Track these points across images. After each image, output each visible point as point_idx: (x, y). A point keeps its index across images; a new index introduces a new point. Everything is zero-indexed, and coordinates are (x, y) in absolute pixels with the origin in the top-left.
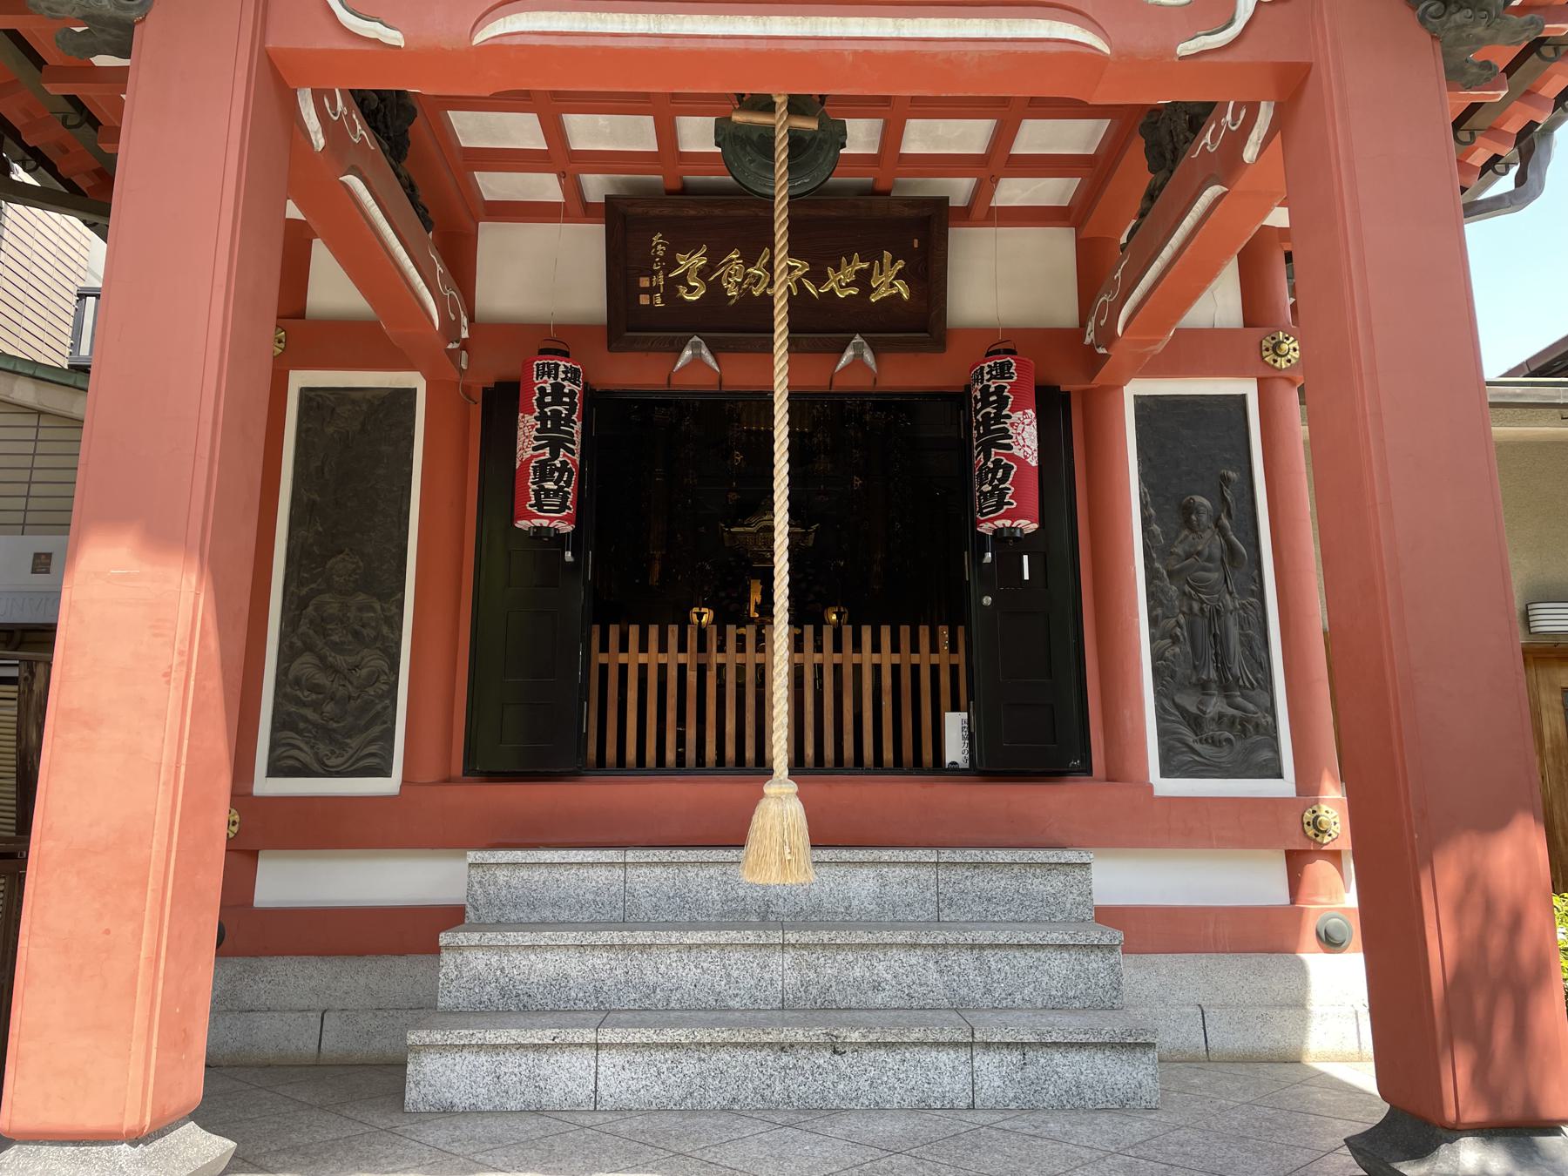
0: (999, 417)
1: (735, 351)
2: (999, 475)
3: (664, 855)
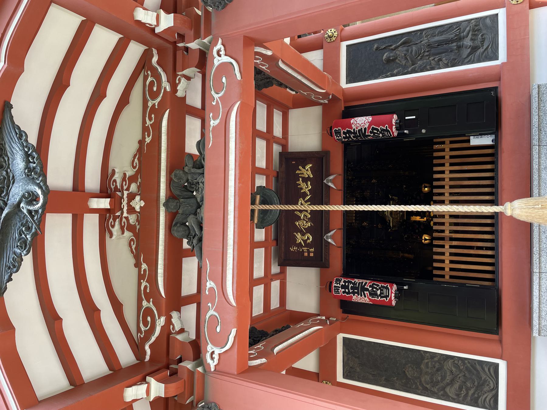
0: (354, 133)
1: (329, 224)
3: (535, 257)
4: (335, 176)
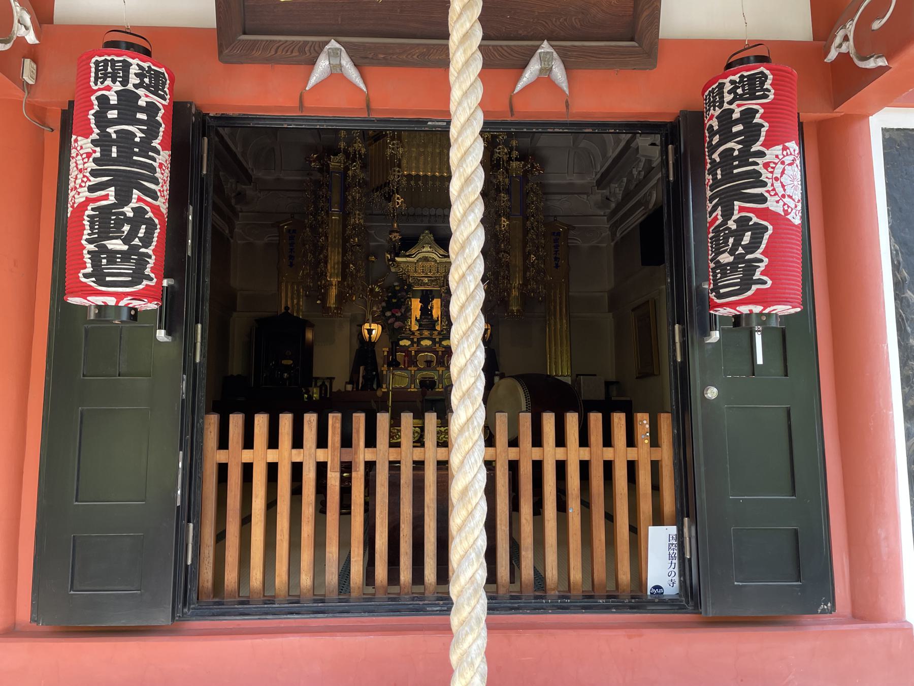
0: (746, 156)
2: (747, 238)
4: (565, 86)
